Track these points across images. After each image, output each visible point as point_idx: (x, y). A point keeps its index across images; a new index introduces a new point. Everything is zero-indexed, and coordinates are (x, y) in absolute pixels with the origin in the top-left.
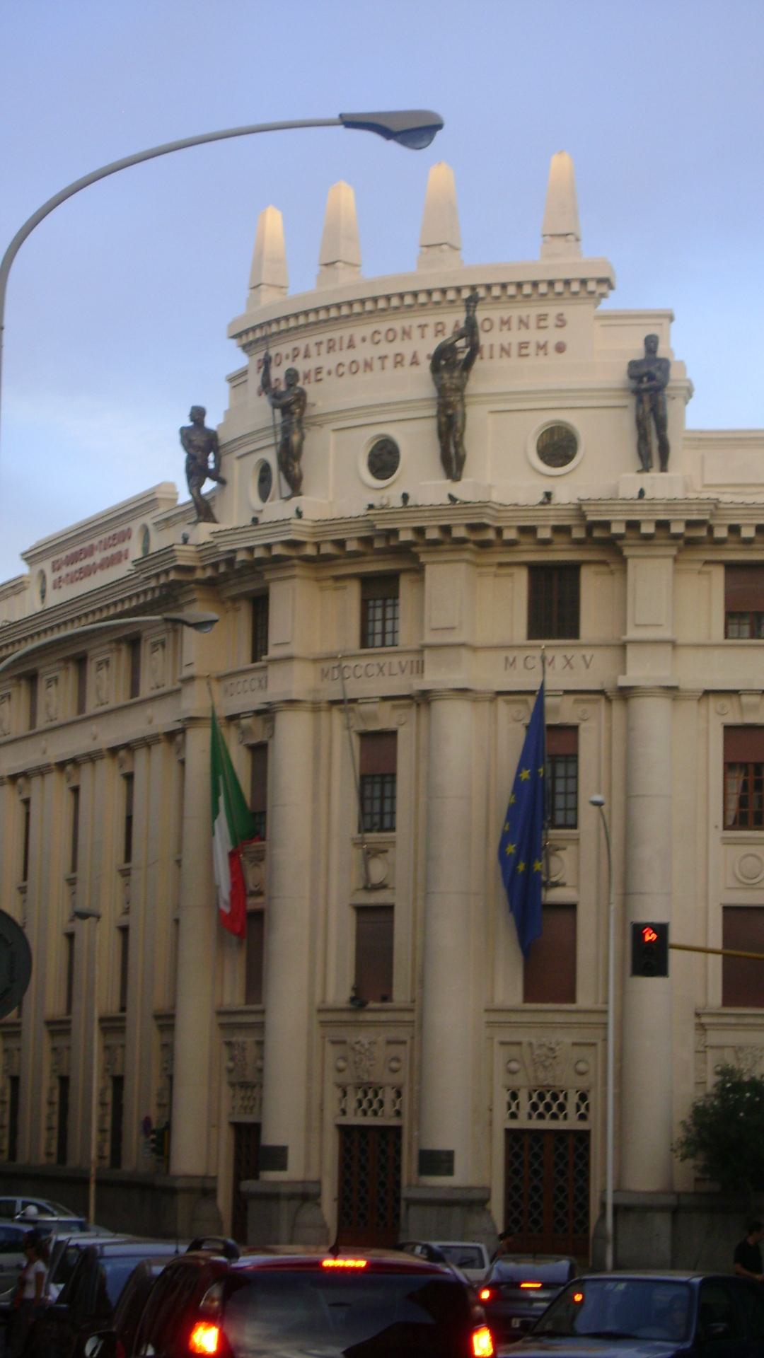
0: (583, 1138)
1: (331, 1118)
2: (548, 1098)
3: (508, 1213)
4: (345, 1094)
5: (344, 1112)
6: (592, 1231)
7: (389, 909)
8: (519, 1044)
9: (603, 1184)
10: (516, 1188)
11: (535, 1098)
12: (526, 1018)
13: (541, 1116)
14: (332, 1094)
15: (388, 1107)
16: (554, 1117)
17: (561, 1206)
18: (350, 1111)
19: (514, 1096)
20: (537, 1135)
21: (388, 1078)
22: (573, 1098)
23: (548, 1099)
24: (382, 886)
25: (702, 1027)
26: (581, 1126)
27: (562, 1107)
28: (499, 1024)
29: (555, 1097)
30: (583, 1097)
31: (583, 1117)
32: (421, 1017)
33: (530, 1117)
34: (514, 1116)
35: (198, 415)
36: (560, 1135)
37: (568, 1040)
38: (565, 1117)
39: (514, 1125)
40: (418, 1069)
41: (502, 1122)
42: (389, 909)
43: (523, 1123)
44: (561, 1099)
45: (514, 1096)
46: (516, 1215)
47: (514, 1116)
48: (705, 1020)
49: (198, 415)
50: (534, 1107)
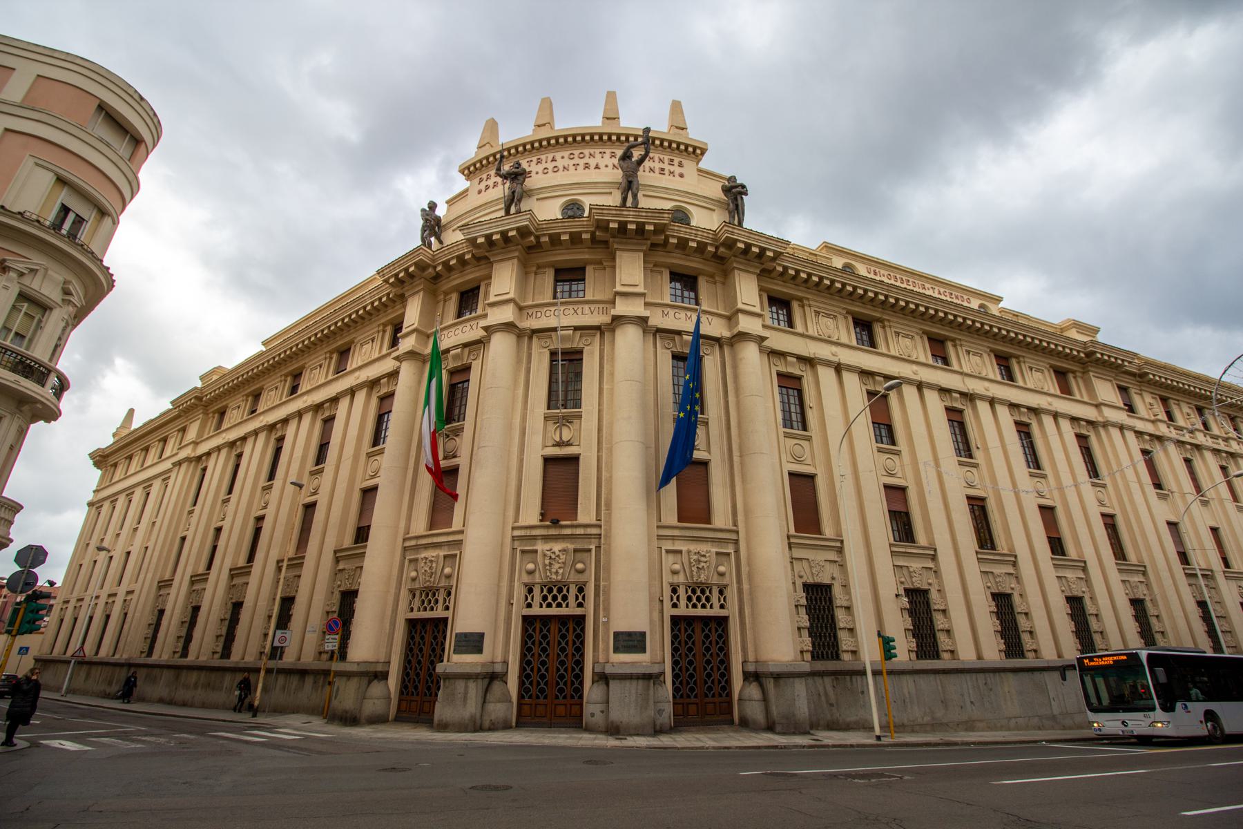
0: (723, 621)
1: (403, 614)
2: (555, 592)
3: (521, 683)
4: (414, 596)
5: (412, 610)
6: (736, 696)
7: (575, 459)
8: (680, 552)
9: (598, 653)
10: (529, 663)
11: (545, 592)
12: (676, 532)
13: (549, 605)
14: (404, 596)
15: (571, 599)
16: (559, 605)
17: (562, 677)
18: (415, 609)
19: (674, 591)
20: (545, 620)
21: (715, 580)
22: (573, 590)
23: (699, 592)
24: (568, 444)
25: (790, 546)
26: (723, 613)
27: (565, 598)
28: (520, 538)
29: (560, 590)
30: (581, 590)
31: (580, 605)
32: (608, 531)
33: (541, 606)
34: (675, 606)
35: (433, 206)
36: (563, 620)
37: (714, 550)
38: (711, 607)
39: (676, 612)
40: (602, 569)
41: (519, 610)
42: (575, 459)
43: (536, 610)
44: (565, 592)
45: (530, 591)
46: (527, 685)
47: (529, 606)
48: (792, 540)
49: (433, 206)
50: (545, 598)
